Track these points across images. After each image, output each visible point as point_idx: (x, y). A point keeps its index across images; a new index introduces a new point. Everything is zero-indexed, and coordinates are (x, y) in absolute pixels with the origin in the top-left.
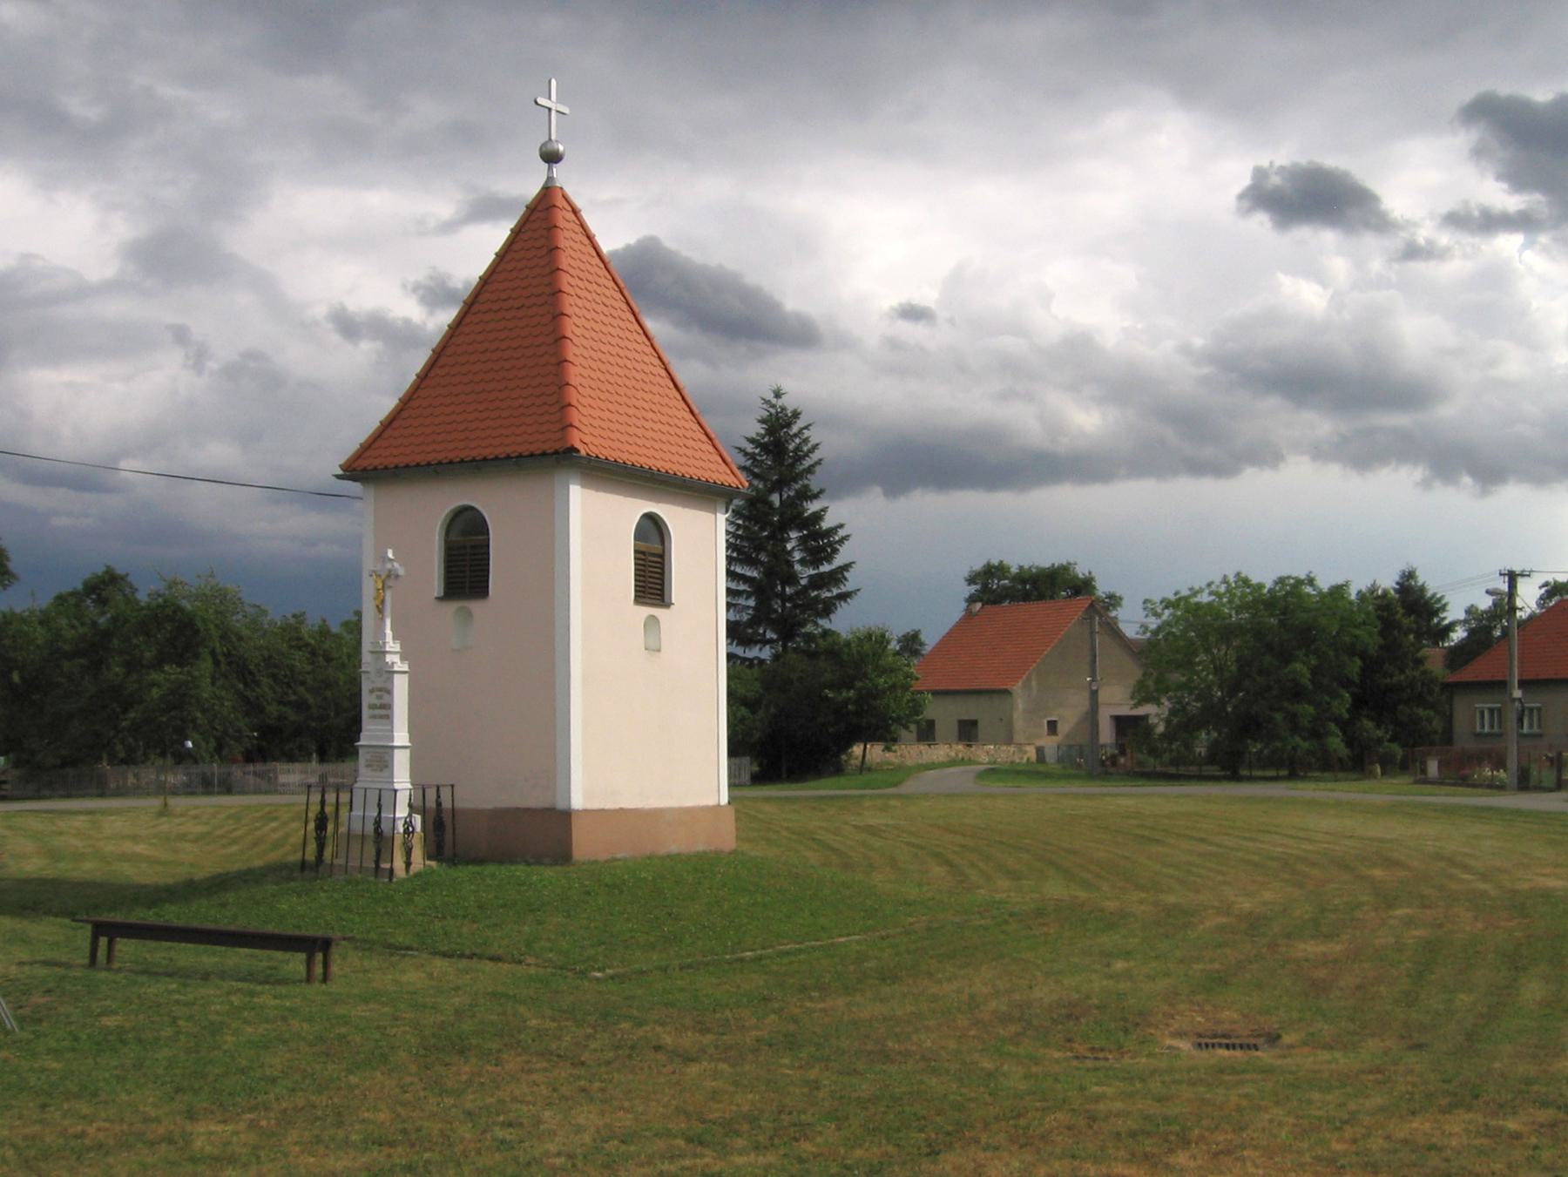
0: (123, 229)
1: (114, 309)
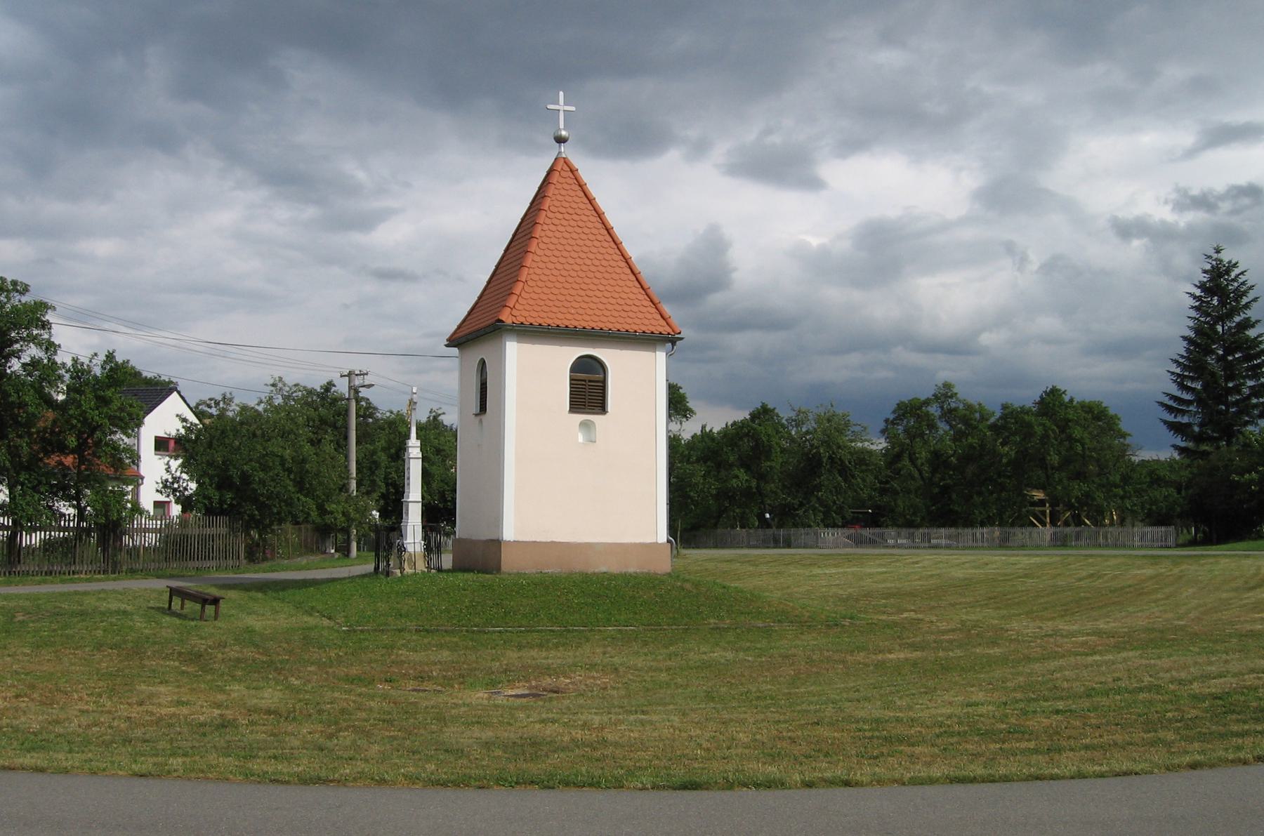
0: (972, 180)
1: (967, 234)
